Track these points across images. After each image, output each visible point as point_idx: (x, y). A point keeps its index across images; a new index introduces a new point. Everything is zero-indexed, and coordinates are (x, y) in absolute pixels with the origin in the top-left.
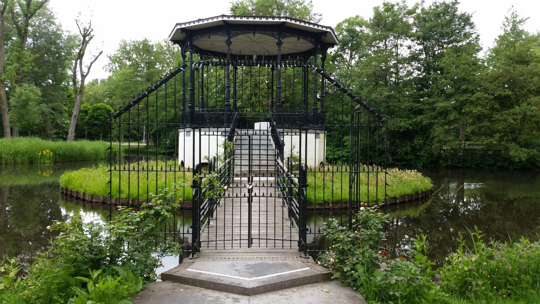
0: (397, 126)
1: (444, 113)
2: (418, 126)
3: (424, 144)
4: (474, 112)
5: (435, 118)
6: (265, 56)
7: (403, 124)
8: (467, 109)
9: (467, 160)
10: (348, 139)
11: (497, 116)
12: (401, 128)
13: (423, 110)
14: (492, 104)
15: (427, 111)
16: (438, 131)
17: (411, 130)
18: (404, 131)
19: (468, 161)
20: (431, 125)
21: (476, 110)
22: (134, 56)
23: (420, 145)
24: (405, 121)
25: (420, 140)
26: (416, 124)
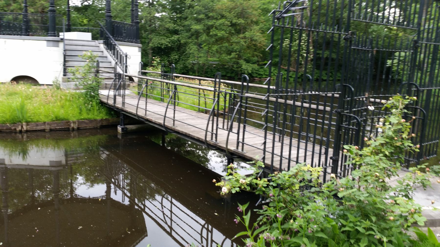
0: (159, 43)
1: (197, 34)
2: (174, 44)
3: (179, 59)
4: (219, 35)
5: (189, 38)
6: (27, 15)
7: (165, 41)
8: (214, 33)
9: (207, 72)
10: (302, 208)
11: (234, 39)
12: (162, 45)
13: (178, 31)
14: (230, 29)
15: (182, 32)
16: (192, 49)
17: (169, 47)
18: (165, 48)
19: (209, 73)
20: (186, 44)
21: (220, 34)
22: (195, 15)
23: (176, 60)
24: (164, 39)
25: (175, 56)
26: (173, 42)
